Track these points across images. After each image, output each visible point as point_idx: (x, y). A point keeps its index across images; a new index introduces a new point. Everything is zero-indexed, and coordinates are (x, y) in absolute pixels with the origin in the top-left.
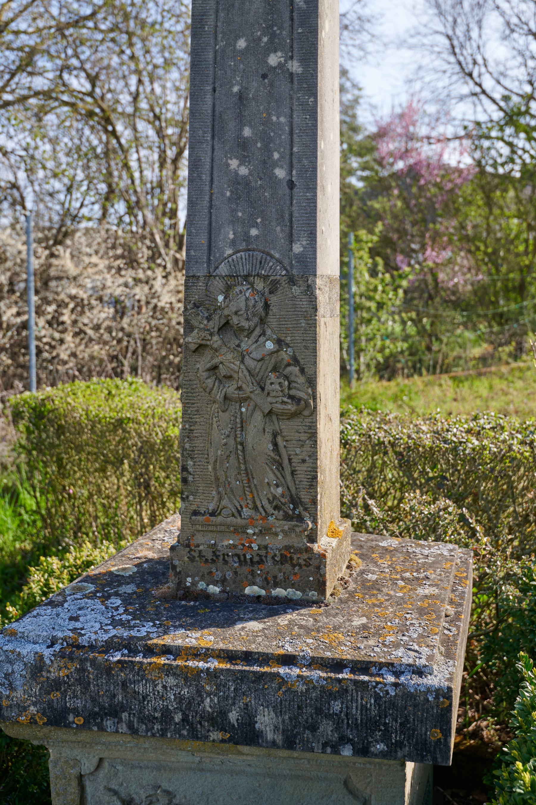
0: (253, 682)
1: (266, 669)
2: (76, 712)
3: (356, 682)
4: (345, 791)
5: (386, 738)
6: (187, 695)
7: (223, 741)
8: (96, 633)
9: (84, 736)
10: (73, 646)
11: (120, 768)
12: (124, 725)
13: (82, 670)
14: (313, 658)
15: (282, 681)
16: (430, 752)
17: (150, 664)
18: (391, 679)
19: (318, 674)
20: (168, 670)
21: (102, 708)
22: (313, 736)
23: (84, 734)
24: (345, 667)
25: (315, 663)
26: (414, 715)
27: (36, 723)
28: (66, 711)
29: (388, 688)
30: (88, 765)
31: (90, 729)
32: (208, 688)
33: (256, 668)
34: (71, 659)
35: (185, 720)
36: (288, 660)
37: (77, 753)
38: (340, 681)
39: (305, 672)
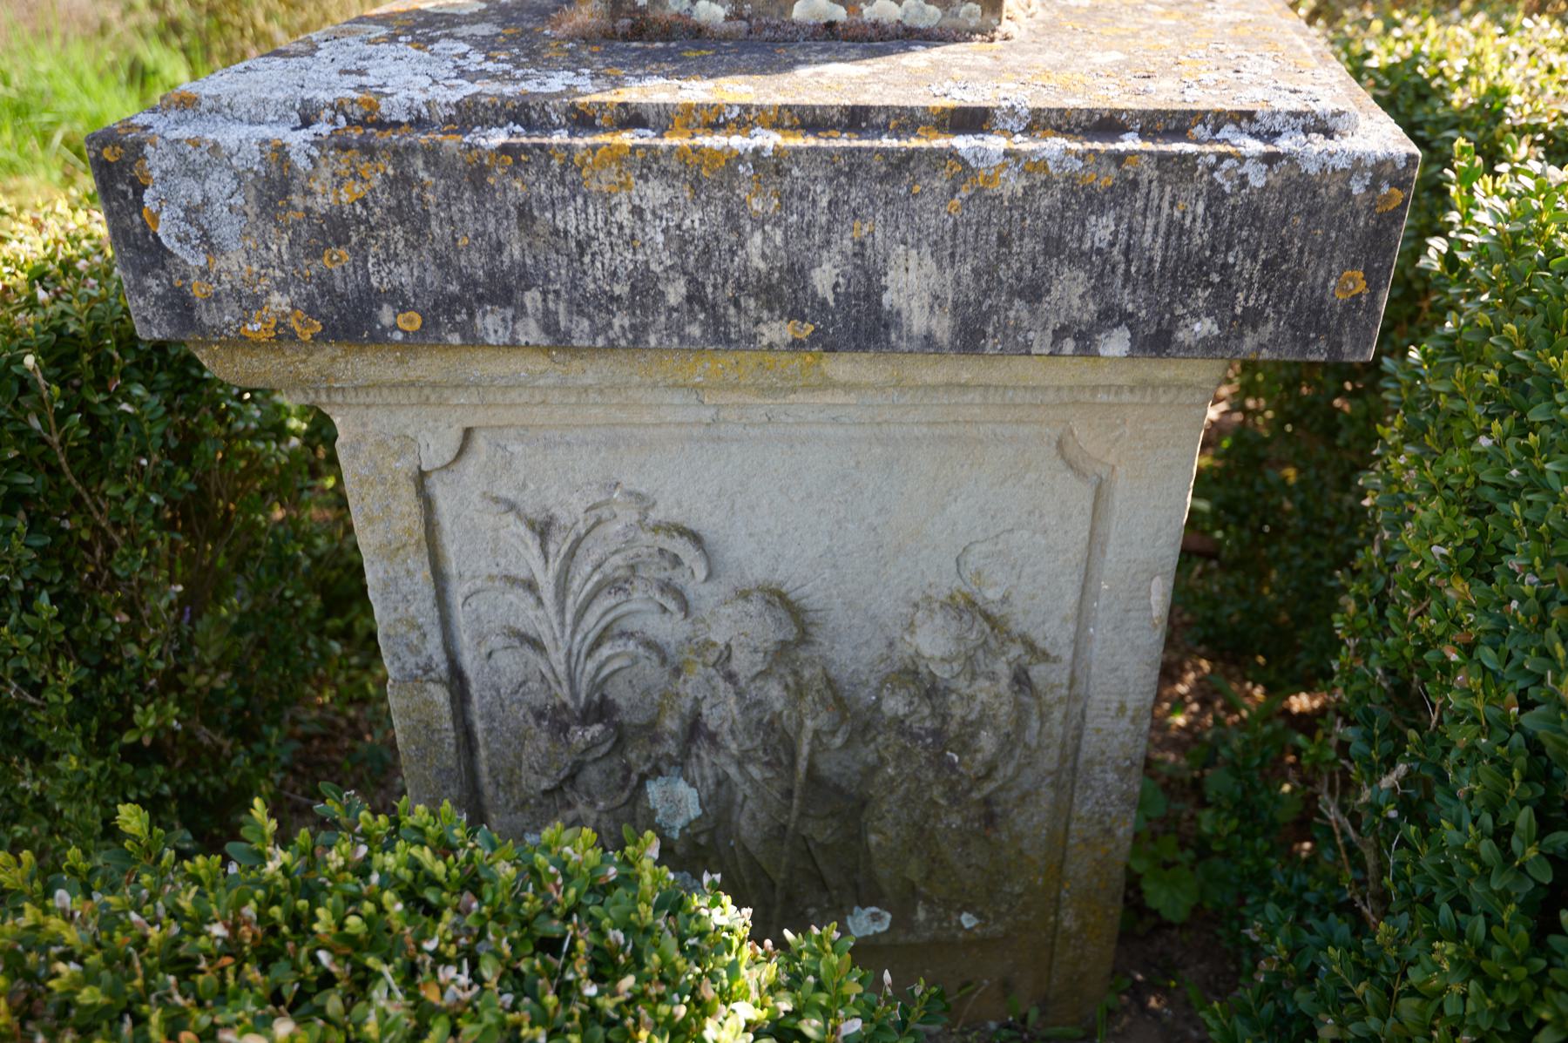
0: (882, 179)
1: (914, 143)
2: (397, 298)
3: (1162, 159)
4: (1059, 463)
5: (1220, 303)
6: (700, 230)
7: (796, 345)
8: (425, 90)
9: (426, 366)
10: (363, 123)
11: (517, 448)
12: (532, 325)
13: (402, 181)
14: (1036, 113)
15: (963, 168)
16: (1326, 329)
17: (594, 148)
18: (1254, 147)
19: (1054, 145)
20: (647, 163)
21: (469, 283)
22: (1033, 312)
23: (424, 361)
24: (1124, 129)
25: (1039, 122)
26: (1304, 238)
27: (293, 336)
28: (369, 299)
29: (1248, 168)
30: (436, 448)
31: (442, 345)
32: (757, 205)
33: (887, 142)
34: (368, 150)
35: (695, 297)
36: (973, 120)
37: (405, 420)
38: (1119, 158)
39: (1024, 144)
